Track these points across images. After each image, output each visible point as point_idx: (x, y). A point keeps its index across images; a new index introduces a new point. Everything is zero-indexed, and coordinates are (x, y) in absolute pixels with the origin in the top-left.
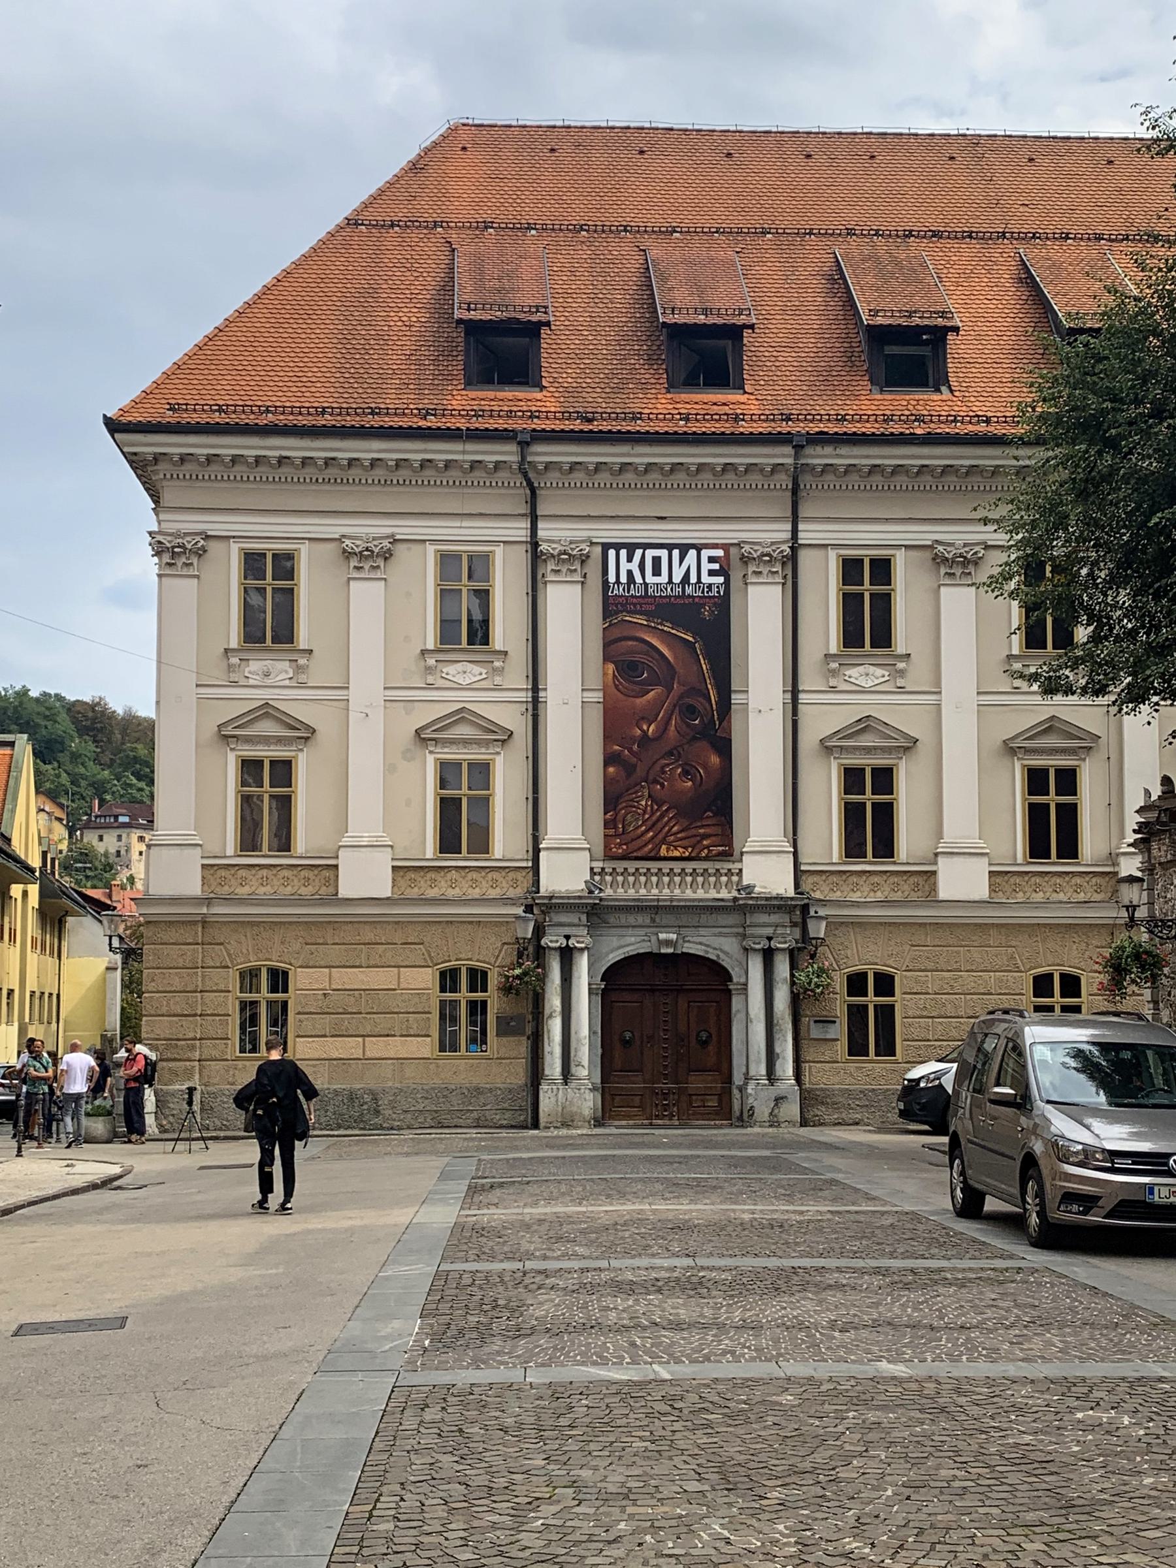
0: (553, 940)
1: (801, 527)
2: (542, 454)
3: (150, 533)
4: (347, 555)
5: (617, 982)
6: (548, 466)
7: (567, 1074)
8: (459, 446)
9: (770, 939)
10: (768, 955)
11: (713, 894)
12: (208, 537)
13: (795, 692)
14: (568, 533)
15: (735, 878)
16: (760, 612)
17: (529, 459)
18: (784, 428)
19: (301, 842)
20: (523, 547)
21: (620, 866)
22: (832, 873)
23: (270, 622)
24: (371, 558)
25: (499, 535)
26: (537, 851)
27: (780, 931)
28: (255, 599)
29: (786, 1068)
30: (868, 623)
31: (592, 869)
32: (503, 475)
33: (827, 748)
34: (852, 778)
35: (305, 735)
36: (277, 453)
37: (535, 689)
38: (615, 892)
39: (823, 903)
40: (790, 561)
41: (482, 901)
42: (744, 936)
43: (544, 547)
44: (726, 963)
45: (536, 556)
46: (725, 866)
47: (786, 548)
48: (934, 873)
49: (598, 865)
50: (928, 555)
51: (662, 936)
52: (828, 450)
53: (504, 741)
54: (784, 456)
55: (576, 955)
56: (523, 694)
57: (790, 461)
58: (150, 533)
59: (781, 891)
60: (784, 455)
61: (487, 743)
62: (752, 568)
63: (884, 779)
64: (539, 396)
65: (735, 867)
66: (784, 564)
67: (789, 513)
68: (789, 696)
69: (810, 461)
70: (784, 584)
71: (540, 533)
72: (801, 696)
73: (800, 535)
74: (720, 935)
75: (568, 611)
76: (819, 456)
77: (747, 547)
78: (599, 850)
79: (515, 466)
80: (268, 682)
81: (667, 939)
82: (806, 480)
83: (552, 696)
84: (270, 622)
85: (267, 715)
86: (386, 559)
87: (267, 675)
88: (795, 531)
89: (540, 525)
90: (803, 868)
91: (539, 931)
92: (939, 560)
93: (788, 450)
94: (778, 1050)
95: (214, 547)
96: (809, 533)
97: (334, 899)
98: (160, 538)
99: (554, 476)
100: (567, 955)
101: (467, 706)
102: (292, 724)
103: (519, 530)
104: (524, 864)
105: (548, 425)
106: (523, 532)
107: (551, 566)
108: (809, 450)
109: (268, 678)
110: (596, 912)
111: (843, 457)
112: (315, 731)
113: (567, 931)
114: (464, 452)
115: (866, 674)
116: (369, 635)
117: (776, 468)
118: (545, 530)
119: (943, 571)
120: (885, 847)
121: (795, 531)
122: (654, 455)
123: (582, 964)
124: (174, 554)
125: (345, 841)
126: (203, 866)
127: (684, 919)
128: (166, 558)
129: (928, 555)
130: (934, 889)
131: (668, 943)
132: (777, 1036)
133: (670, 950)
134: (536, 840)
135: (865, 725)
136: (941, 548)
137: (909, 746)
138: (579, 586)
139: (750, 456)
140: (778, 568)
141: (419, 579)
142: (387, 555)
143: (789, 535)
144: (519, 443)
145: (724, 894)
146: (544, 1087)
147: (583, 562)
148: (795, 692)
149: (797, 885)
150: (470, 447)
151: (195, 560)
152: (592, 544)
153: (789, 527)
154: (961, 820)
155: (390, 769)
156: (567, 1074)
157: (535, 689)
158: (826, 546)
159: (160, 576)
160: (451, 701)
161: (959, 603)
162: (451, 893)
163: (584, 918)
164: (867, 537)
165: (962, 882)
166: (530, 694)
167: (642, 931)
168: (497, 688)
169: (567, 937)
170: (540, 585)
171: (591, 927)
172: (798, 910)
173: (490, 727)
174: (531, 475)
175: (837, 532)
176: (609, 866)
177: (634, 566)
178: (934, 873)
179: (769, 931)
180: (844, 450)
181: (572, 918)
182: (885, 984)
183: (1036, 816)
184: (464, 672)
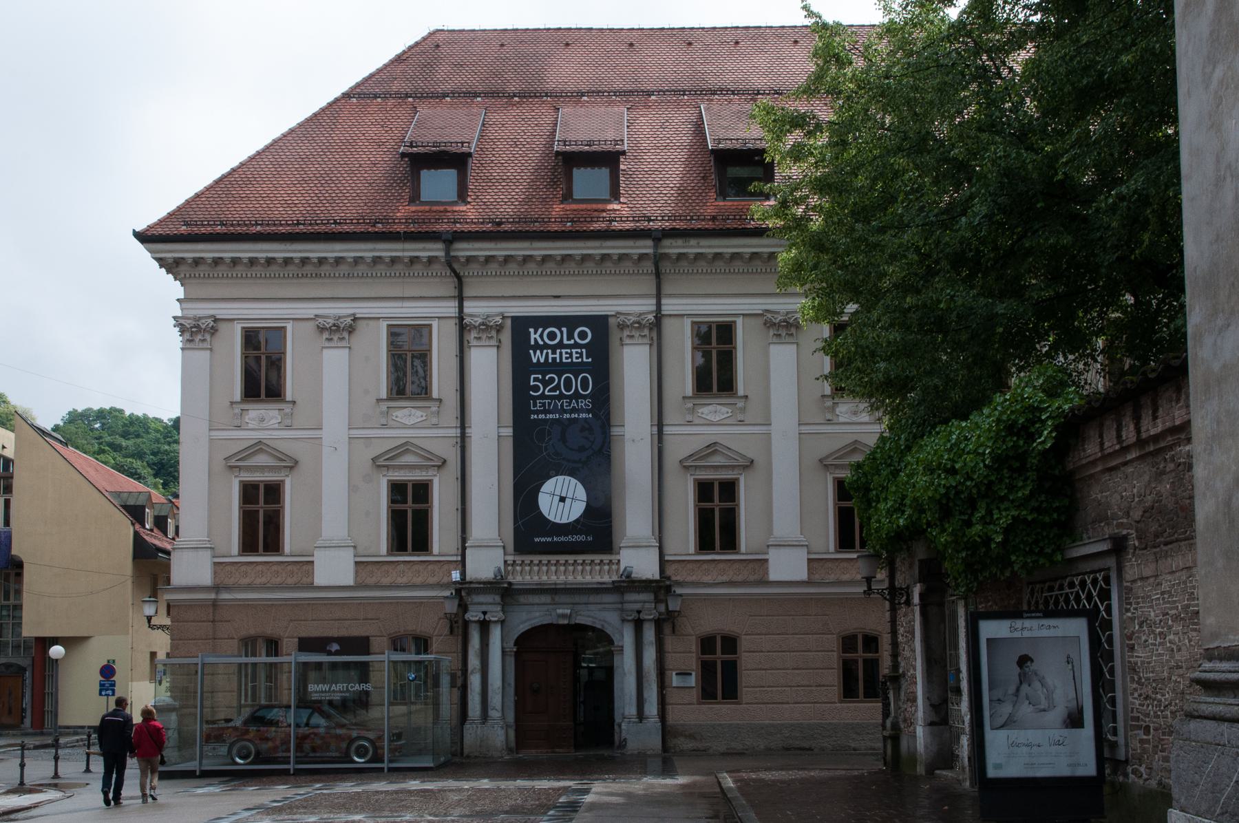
0: (473, 615)
1: (664, 301)
2: (464, 250)
3: (175, 318)
4: (321, 329)
5: (529, 647)
6: (469, 260)
7: (485, 716)
8: (399, 246)
9: (639, 612)
10: (638, 625)
11: (598, 579)
12: (216, 320)
13: (660, 425)
14: (485, 310)
15: (614, 567)
16: (633, 364)
17: (452, 254)
18: (644, 225)
19: (288, 543)
20: (453, 322)
21: (527, 559)
22: (689, 561)
23: (262, 378)
24: (340, 331)
25: (430, 308)
26: (464, 549)
27: (647, 605)
28: (252, 363)
29: (652, 709)
30: (716, 373)
31: (505, 562)
32: (436, 267)
33: (686, 465)
34: (704, 490)
35: (292, 465)
36: (264, 255)
37: (463, 427)
38: (520, 578)
39: (680, 584)
40: (656, 325)
41: (839, 583)
42: (622, 610)
43: (467, 320)
44: (609, 630)
45: (463, 327)
46: (606, 558)
47: (651, 317)
48: (766, 560)
49: (510, 558)
50: (760, 321)
51: (560, 611)
52: (680, 242)
53: (439, 467)
54: (645, 247)
55: (492, 626)
56: (454, 431)
57: (650, 251)
58: (175, 318)
59: (650, 577)
60: (645, 247)
61: (427, 467)
62: (626, 332)
63: (729, 489)
64: (464, 208)
65: (614, 558)
66: (651, 329)
67: (654, 292)
68: (655, 429)
69: (667, 251)
70: (651, 345)
71: (466, 310)
72: (665, 429)
73: (663, 308)
74: (604, 609)
75: (488, 368)
76: (673, 247)
77: (622, 317)
78: (511, 547)
79: (443, 260)
80: (264, 425)
81: (561, 613)
82: (666, 267)
83: (474, 432)
84: (262, 378)
85: (261, 450)
86: (350, 333)
87: (262, 420)
88: (659, 305)
89: (466, 304)
90: (667, 558)
91: (464, 607)
92: (769, 325)
93: (649, 243)
94: (645, 695)
95: (223, 327)
96: (669, 306)
97: (311, 587)
98: (182, 321)
99: (474, 268)
100: (484, 626)
101: (412, 440)
102: (280, 456)
103: (450, 308)
104: (454, 558)
105: (466, 228)
106: (453, 310)
107: (474, 334)
108: (666, 242)
109: (263, 420)
110: (504, 590)
111: (693, 247)
112: (296, 462)
113: (484, 608)
114: (403, 250)
115: (714, 411)
116: (335, 384)
117: (642, 257)
118: (470, 307)
119: (771, 333)
120: (730, 542)
121: (659, 305)
122: (588, 248)
123: (496, 635)
124: (194, 331)
125: (319, 543)
126: (356, 563)
127: (577, 599)
128: (187, 336)
129: (760, 321)
130: (766, 573)
131: (564, 616)
132: (645, 685)
133: (566, 622)
134: (464, 540)
135: (713, 448)
136: (769, 316)
137: (749, 465)
138: (495, 349)
139: (545, 249)
140: (646, 332)
141: (375, 348)
142: (351, 330)
143: (654, 308)
144: (444, 241)
145: (606, 579)
146: (467, 726)
147: (498, 331)
148: (660, 425)
149: (662, 571)
150: (408, 246)
151: (208, 337)
152: (504, 318)
153: (654, 301)
154: (786, 522)
155: (352, 489)
156: (485, 716)
157: (463, 427)
158: (682, 315)
159: (183, 349)
160: (398, 435)
161: (783, 357)
162: (400, 580)
163: (498, 599)
164: (715, 307)
165: (787, 567)
166: (459, 431)
167: (546, 608)
168: (435, 426)
169: (485, 613)
170: (466, 349)
171: (504, 606)
172: (661, 588)
173: (428, 456)
174: (456, 266)
175: (692, 304)
176: (519, 559)
177: (537, 336)
178: (766, 560)
179: (638, 606)
180: (693, 242)
181: (488, 598)
182: (730, 643)
183: (248, 520)
184: (409, 415)
